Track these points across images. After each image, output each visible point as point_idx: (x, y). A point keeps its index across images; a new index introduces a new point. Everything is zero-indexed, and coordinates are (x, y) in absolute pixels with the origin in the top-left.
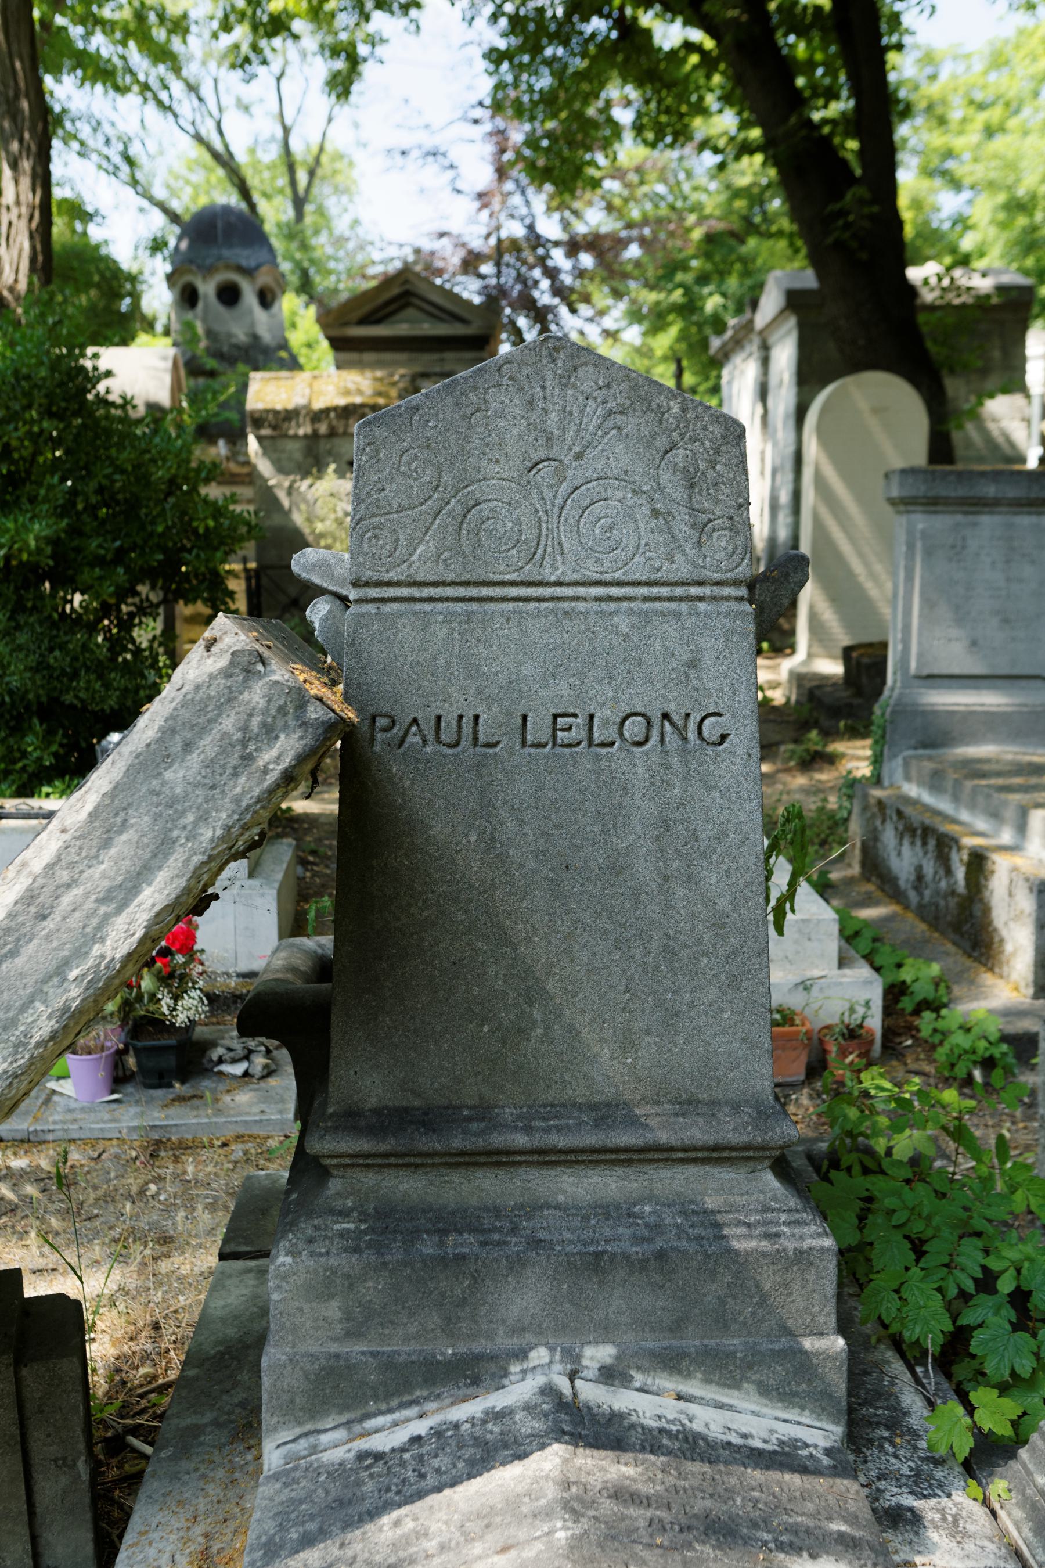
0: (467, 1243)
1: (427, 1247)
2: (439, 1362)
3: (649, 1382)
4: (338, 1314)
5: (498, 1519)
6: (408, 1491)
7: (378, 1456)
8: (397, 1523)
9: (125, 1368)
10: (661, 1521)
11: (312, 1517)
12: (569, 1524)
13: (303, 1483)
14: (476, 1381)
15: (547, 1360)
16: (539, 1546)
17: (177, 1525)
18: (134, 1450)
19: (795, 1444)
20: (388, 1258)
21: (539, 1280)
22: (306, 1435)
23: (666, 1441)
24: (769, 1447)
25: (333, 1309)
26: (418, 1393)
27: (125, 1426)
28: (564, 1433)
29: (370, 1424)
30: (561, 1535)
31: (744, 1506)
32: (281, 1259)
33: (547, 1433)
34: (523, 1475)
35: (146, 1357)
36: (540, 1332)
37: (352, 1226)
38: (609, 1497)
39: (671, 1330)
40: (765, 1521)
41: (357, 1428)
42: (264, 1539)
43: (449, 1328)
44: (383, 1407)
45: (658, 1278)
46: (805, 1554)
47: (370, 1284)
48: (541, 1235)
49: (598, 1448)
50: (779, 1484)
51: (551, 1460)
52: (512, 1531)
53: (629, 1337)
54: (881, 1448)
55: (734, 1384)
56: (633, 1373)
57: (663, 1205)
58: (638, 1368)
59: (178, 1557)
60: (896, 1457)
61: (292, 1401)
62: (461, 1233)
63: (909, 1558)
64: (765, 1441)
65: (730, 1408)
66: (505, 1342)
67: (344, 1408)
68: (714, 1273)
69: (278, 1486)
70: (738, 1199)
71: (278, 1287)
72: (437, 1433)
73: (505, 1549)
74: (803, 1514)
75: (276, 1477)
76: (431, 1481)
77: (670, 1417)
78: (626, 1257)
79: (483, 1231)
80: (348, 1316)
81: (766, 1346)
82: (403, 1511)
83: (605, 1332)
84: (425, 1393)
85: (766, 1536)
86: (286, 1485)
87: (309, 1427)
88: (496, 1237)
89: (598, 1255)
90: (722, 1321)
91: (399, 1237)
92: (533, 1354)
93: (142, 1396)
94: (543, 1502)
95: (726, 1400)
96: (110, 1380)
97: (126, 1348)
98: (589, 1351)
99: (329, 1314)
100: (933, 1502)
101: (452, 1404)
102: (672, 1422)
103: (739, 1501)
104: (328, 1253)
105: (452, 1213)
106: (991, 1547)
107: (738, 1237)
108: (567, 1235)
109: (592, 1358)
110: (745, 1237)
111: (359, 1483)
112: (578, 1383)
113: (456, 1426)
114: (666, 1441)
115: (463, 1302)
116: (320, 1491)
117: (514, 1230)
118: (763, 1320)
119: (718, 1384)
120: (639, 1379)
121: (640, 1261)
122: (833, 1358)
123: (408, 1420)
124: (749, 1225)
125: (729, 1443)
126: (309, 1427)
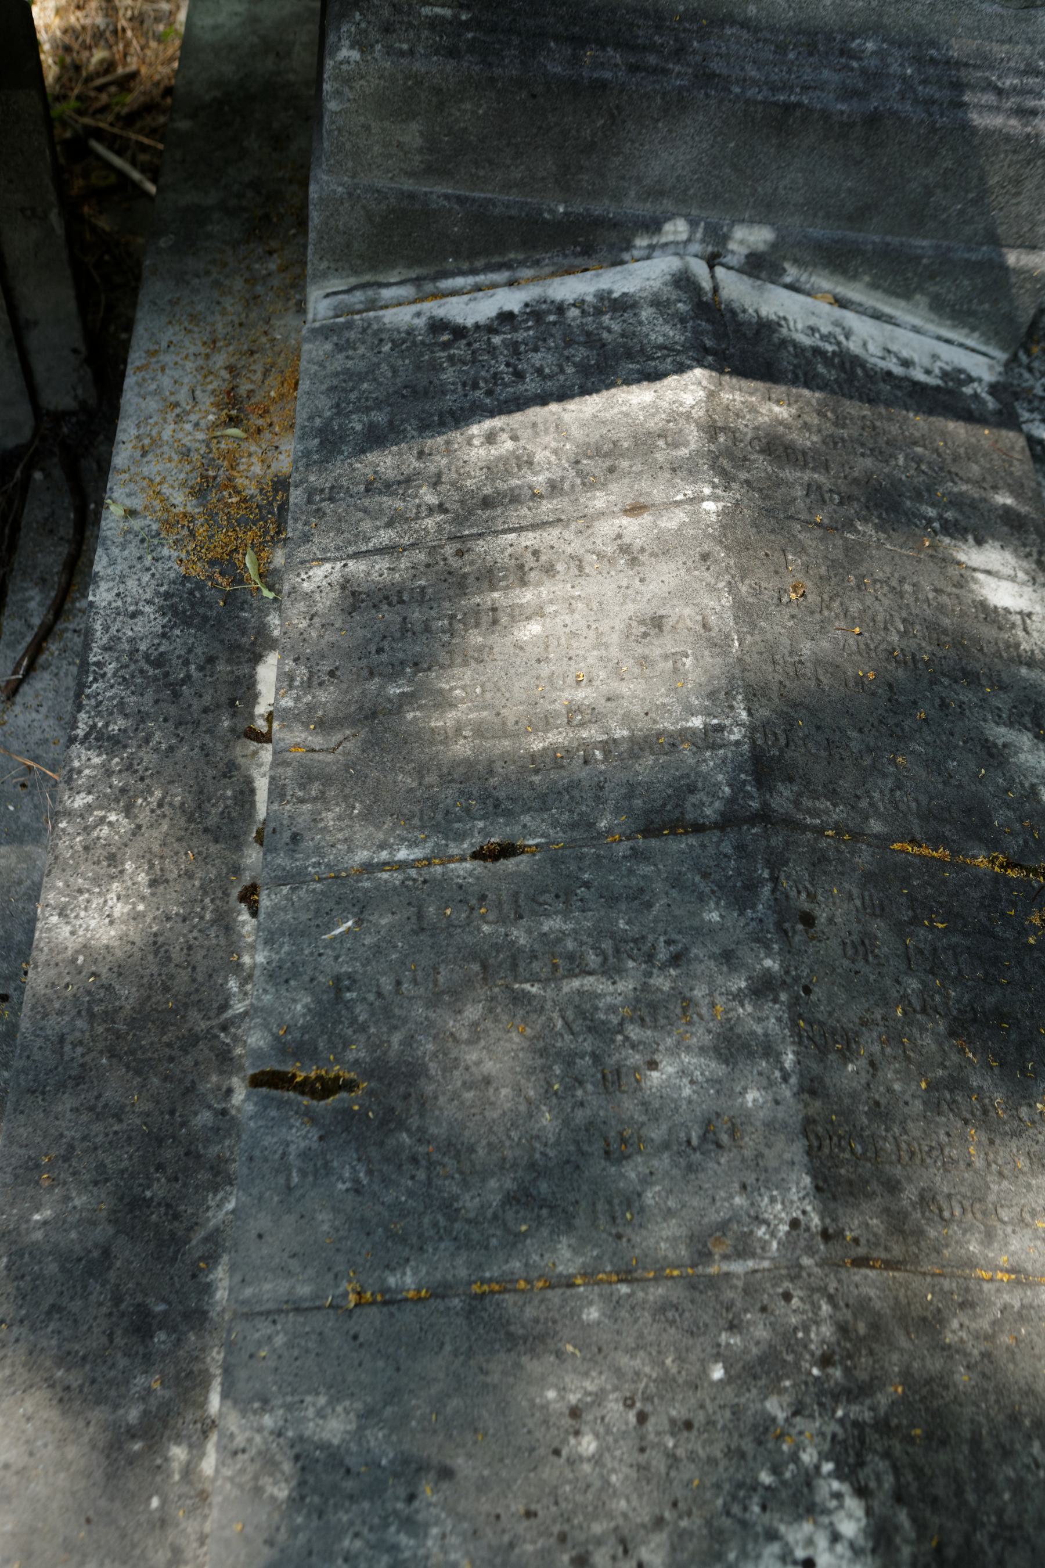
0: (607, 63)
1: (555, 64)
2: (545, 222)
3: (803, 278)
4: (419, 142)
5: (625, 464)
7: (459, 332)
8: (491, 438)
9: (76, 46)
10: (819, 487)
11: (378, 405)
12: (719, 492)
13: (362, 350)
14: (588, 251)
15: (684, 237)
16: (680, 516)
17: (192, 349)
18: (99, 157)
19: (956, 377)
23: (821, 369)
24: (932, 381)
25: (412, 134)
26: (512, 256)
27: (86, 127)
28: (707, 351)
31: (906, 468)
32: (344, 53)
33: (685, 350)
34: (654, 405)
35: (99, 35)
37: (447, 12)
38: (762, 451)
41: (429, 287)
42: (318, 421)
44: (465, 266)
47: (468, 106)
48: (716, 66)
50: (943, 434)
51: (689, 390)
52: (644, 484)
55: (904, 292)
57: (892, 43)
59: (198, 393)
60: (1030, 370)
61: (348, 246)
62: (603, 48)
64: (928, 372)
65: (890, 320)
66: (635, 207)
67: (412, 262)
69: (328, 347)
70: (996, 47)
71: (338, 93)
72: (535, 313)
74: (968, 481)
76: (531, 385)
77: (824, 330)
78: (826, 115)
82: (497, 422)
83: (765, 211)
85: (931, 512)
86: (339, 348)
87: (367, 278)
88: (652, 59)
89: (788, 108)
91: (516, 41)
92: (668, 227)
93: (101, 89)
94: (684, 452)
95: (887, 310)
96: (61, 63)
97: (72, 19)
98: (740, 233)
99: (406, 139)
101: (553, 274)
102: (824, 338)
103: (901, 461)
104: (411, 52)
107: (982, 108)
109: (742, 242)
110: (990, 108)
111: (435, 367)
113: (560, 309)
114: (821, 369)
116: (384, 367)
117: (680, 52)
120: (792, 273)
123: (494, 286)
124: (1000, 92)
125: (889, 373)
126: (367, 278)
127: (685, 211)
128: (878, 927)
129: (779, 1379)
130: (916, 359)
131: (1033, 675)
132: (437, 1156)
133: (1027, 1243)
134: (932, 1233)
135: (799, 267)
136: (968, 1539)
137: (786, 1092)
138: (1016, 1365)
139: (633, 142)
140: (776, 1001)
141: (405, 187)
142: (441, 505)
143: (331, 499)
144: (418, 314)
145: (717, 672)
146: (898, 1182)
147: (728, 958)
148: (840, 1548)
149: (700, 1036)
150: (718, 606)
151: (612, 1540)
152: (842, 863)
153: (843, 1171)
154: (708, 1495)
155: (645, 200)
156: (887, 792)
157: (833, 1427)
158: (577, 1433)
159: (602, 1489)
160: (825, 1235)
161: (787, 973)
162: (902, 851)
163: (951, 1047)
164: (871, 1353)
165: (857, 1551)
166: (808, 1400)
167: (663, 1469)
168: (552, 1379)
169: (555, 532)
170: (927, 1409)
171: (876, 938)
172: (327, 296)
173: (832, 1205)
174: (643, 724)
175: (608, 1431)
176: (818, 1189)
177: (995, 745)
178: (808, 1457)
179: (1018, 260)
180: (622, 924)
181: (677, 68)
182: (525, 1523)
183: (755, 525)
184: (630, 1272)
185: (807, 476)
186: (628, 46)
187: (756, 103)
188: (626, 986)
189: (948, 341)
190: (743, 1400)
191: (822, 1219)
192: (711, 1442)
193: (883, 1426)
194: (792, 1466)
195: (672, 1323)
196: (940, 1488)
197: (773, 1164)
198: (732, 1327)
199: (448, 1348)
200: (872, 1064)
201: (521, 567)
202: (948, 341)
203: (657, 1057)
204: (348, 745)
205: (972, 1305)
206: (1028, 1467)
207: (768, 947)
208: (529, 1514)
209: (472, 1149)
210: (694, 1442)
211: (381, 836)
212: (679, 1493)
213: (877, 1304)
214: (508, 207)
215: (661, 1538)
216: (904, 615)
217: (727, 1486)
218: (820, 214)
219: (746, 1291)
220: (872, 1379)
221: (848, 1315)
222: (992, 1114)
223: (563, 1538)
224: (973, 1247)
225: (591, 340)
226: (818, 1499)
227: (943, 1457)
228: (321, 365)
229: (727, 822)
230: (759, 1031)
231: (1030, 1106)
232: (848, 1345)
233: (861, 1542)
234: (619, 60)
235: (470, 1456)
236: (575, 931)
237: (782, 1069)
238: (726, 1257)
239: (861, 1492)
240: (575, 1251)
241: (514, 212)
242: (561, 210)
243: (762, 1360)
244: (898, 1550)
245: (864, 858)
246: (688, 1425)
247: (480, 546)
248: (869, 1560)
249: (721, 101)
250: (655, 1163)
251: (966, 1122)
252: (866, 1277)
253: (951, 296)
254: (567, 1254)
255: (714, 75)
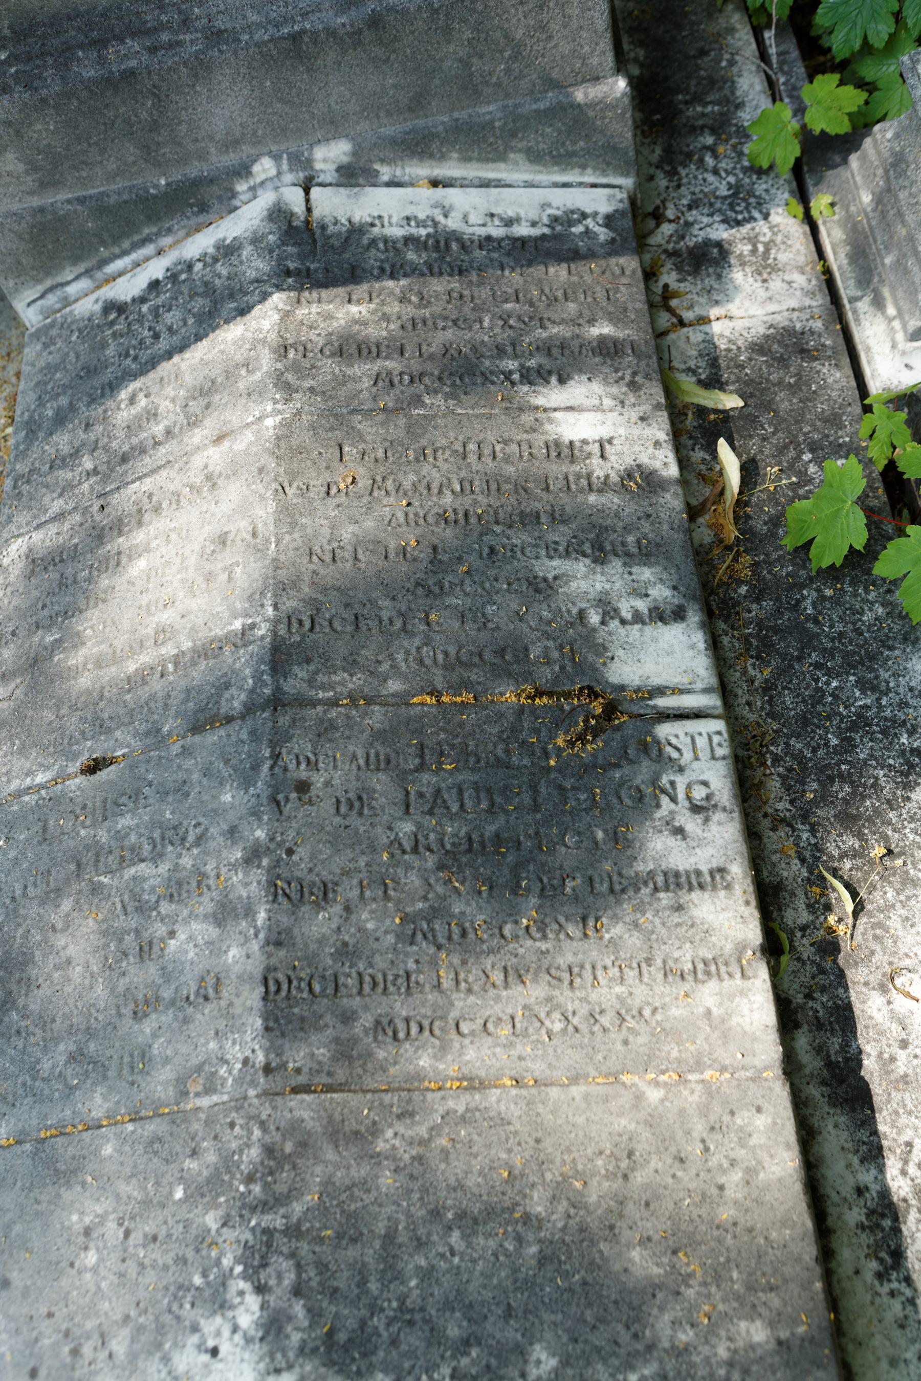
0: (129, 53)
1: (87, 69)
2: (154, 197)
3: (398, 172)
4: (21, 167)
6: (144, 356)
8: (132, 400)
10: (389, 373)
14: (203, 208)
15: (273, 172)
20: (44, 92)
21: (234, 82)
22: (51, 289)
23: (411, 256)
26: (146, 231)
28: (288, 273)
29: (112, 268)
30: (270, 422)
34: (243, 338)
36: (257, 142)
39: (410, 109)
40: (514, 345)
41: (99, 275)
43: (150, 155)
44: (117, 250)
45: (379, 51)
46: (554, 380)
47: (38, 127)
48: (221, 23)
49: (325, 286)
53: (363, 126)
54: (701, 162)
55: (499, 156)
56: (377, 166)
58: (382, 161)
60: (716, 172)
62: (122, 41)
63: (704, 313)
64: (534, 224)
67: (76, 259)
68: (447, 31)
72: (173, 276)
73: (219, 439)
74: (563, 321)
75: (37, 335)
78: (331, 33)
79: (148, 32)
80: (34, 167)
81: (529, 107)
83: (333, 127)
84: (154, 229)
86: (46, 346)
87: (49, 283)
88: (165, 37)
89: (295, 38)
90: (470, 88)
92: (256, 168)
95: (492, 175)
99: (10, 168)
100: (745, 230)
101: (188, 235)
105: (104, 15)
106: (800, 280)
108: (253, 17)
109: (325, 160)
111: (104, 345)
112: (315, 192)
113: (190, 266)
114: (411, 256)
115: (154, 126)
118: (521, 76)
119: (479, 160)
120: (385, 172)
121: (351, 35)
122: (613, 107)
123: (147, 259)
125: (489, 238)
126: (49, 283)
127: (265, 150)
128: (380, 782)
129: (218, 1195)
130: (523, 215)
131: (603, 500)
132: (31, 1029)
133: (486, 1051)
134: (381, 1054)
135: (389, 164)
136: (363, 1324)
137: (255, 946)
138: (448, 1164)
139: (186, 109)
140: (258, 867)
141: (35, 204)
142: (95, 469)
143: (28, 482)
144: (97, 301)
145: (256, 575)
146: (354, 1012)
147: (232, 833)
148: (238, 1338)
149: (207, 905)
150: (265, 512)
151: (96, 1336)
152: (351, 728)
153: (296, 1010)
154: (160, 1295)
155: (227, 152)
156: (413, 651)
157: (247, 1236)
158: (86, 1248)
159: (95, 1293)
160: (267, 1069)
161: (272, 839)
162: (423, 704)
163: (437, 880)
164: (294, 1167)
165: (248, 1340)
166: (233, 1213)
167: (134, 1275)
168: (77, 1205)
169: (164, 473)
170: (343, 1212)
171: (374, 791)
172: (29, 305)
173: (279, 1042)
174: (203, 634)
175: (105, 1247)
176: (267, 1029)
177: (545, 580)
178: (226, 1262)
179: (586, 95)
180: (168, 816)
181: (188, 37)
182: (47, 1322)
183: (313, 428)
184: (137, 1113)
185: (376, 367)
186: (136, 34)
187: (265, 43)
188: (164, 868)
189: (565, 185)
190: (191, 1216)
191: (266, 1056)
192: (167, 1252)
193: (294, 1231)
194: (215, 1270)
195: (156, 1153)
196: (342, 1282)
197: (237, 1010)
198: (194, 1153)
199: (19, 1184)
200: (347, 909)
201: (140, 511)
202: (565, 185)
203: (176, 927)
204: (18, 692)
205: (412, 1114)
206: (442, 1256)
207: (260, 819)
208: (50, 1315)
209: (53, 1021)
210: (156, 1254)
211: (28, 765)
212: (142, 1294)
213: (309, 1124)
214: (119, 194)
215: (125, 1333)
216: (463, 474)
217: (172, 1288)
218: (382, 114)
219: (207, 1123)
220: (290, 1191)
221: (277, 1137)
222: (471, 936)
223: (67, 1334)
224: (425, 1062)
225: (208, 289)
226: (228, 1297)
227: (352, 1253)
228: (33, 365)
229: (249, 709)
230: (245, 895)
231: (516, 922)
232: (272, 1163)
233: (252, 1332)
234: (137, 48)
235: (21, 1270)
236: (138, 826)
237: (255, 927)
238: (197, 1095)
239: (260, 1289)
240: (105, 1097)
241: (125, 197)
242: (163, 182)
243: (208, 1181)
244: (288, 1337)
245: (377, 717)
246: (155, 1238)
247: (115, 499)
248: (257, 1346)
249: (235, 52)
250: (163, 1018)
251: (439, 947)
252: (302, 1101)
253: (541, 146)
254: (98, 1100)
255: (220, 32)
